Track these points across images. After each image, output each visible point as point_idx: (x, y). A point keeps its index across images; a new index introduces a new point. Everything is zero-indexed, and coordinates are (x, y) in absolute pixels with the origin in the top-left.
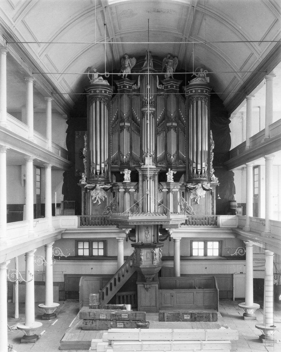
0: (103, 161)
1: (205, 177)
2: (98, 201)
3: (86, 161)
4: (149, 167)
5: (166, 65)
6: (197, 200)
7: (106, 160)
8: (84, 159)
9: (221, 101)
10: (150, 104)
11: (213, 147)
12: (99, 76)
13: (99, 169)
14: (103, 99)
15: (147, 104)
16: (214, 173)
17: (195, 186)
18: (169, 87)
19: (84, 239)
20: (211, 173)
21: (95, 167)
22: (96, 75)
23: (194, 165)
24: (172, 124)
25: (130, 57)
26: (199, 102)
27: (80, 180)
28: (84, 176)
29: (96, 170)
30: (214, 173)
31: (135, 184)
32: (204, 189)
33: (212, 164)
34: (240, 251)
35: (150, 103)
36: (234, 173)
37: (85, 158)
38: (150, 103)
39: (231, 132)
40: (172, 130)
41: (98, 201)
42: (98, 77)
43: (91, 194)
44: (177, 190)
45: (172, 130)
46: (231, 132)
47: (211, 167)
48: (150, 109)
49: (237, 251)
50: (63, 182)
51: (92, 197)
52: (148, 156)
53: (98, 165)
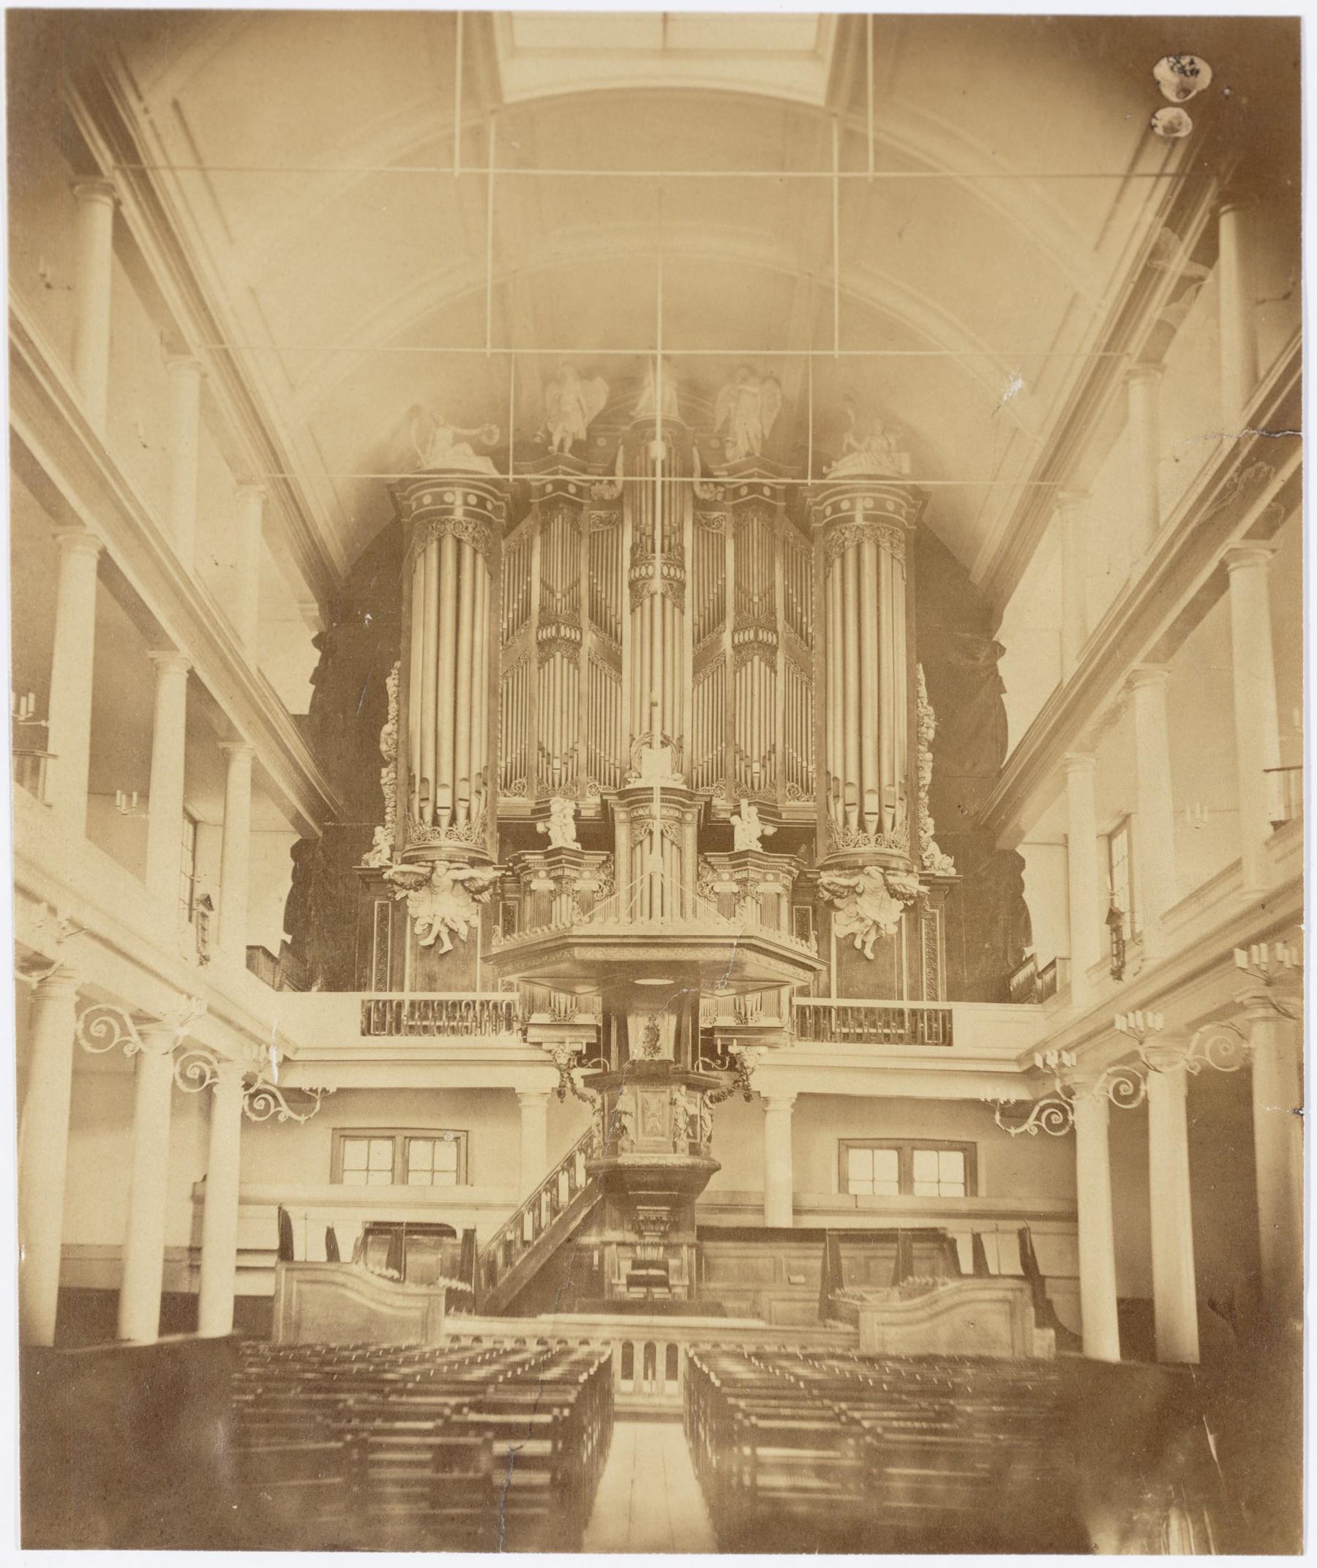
0: (462, 773)
1: (894, 844)
2: (438, 937)
3: (393, 775)
4: (657, 784)
5: (732, 405)
6: (864, 943)
7: (476, 768)
8: (384, 771)
9: (963, 573)
10: (663, 551)
11: (931, 735)
12: (457, 439)
13: (449, 804)
14: (470, 529)
15: (653, 551)
16: (934, 838)
17: (852, 882)
18: (744, 491)
19: (403, 643)
20: (922, 833)
21: (431, 797)
22: (445, 434)
23: (851, 795)
24: (756, 635)
25: (587, 375)
26: (868, 552)
27: (365, 856)
28: (382, 837)
29: (435, 808)
30: (934, 838)
31: (597, 858)
32: (894, 894)
33: (927, 800)
34: (1048, 1118)
35: (666, 549)
36: (1022, 861)
37: (386, 764)
38: (666, 549)
39: (1005, 692)
40: (756, 659)
41: (438, 937)
42: (453, 445)
43: (411, 911)
44: (780, 889)
45: (756, 659)
46: (1005, 692)
47: (924, 812)
48: (665, 573)
49: (1038, 1118)
50: (290, 884)
51: (414, 920)
52: (657, 744)
53: (445, 786)
